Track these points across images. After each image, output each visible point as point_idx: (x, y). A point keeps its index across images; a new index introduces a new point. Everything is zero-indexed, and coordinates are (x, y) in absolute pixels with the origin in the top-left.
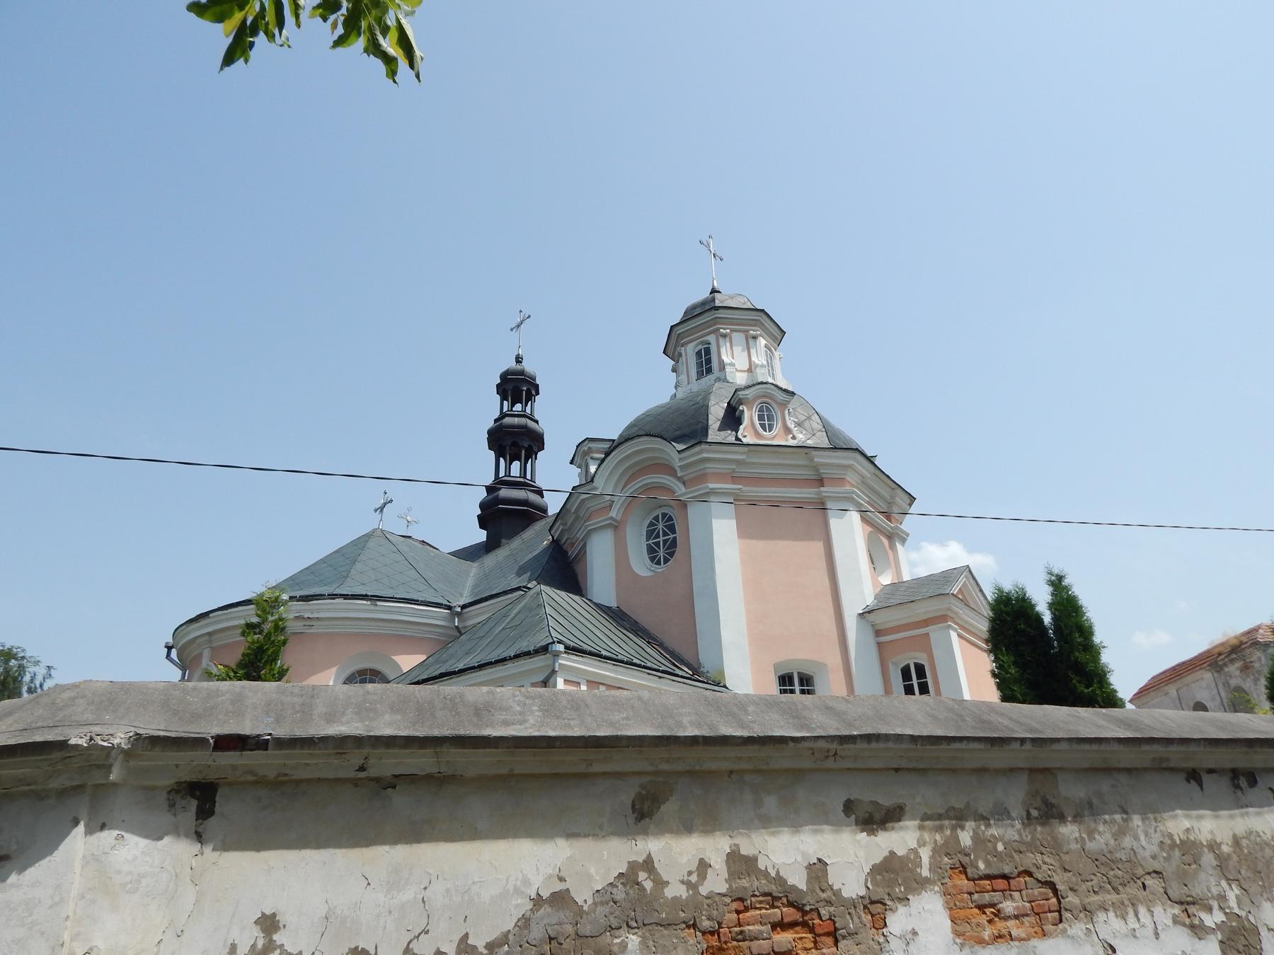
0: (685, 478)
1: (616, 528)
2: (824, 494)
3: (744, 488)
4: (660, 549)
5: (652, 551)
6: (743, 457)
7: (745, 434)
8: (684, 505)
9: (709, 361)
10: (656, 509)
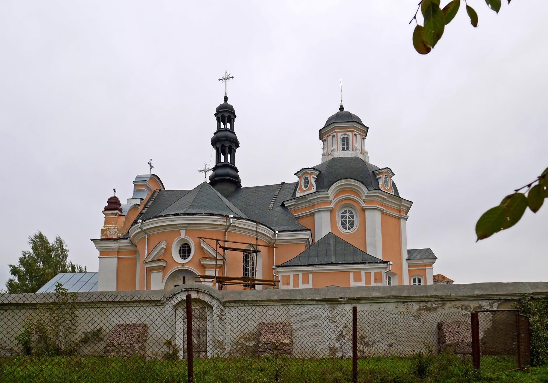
0: (365, 200)
1: (331, 211)
2: (364, 208)
3: (385, 210)
4: (347, 224)
5: (342, 223)
6: (386, 197)
7: (382, 187)
8: (364, 210)
9: (347, 144)
10: (345, 207)
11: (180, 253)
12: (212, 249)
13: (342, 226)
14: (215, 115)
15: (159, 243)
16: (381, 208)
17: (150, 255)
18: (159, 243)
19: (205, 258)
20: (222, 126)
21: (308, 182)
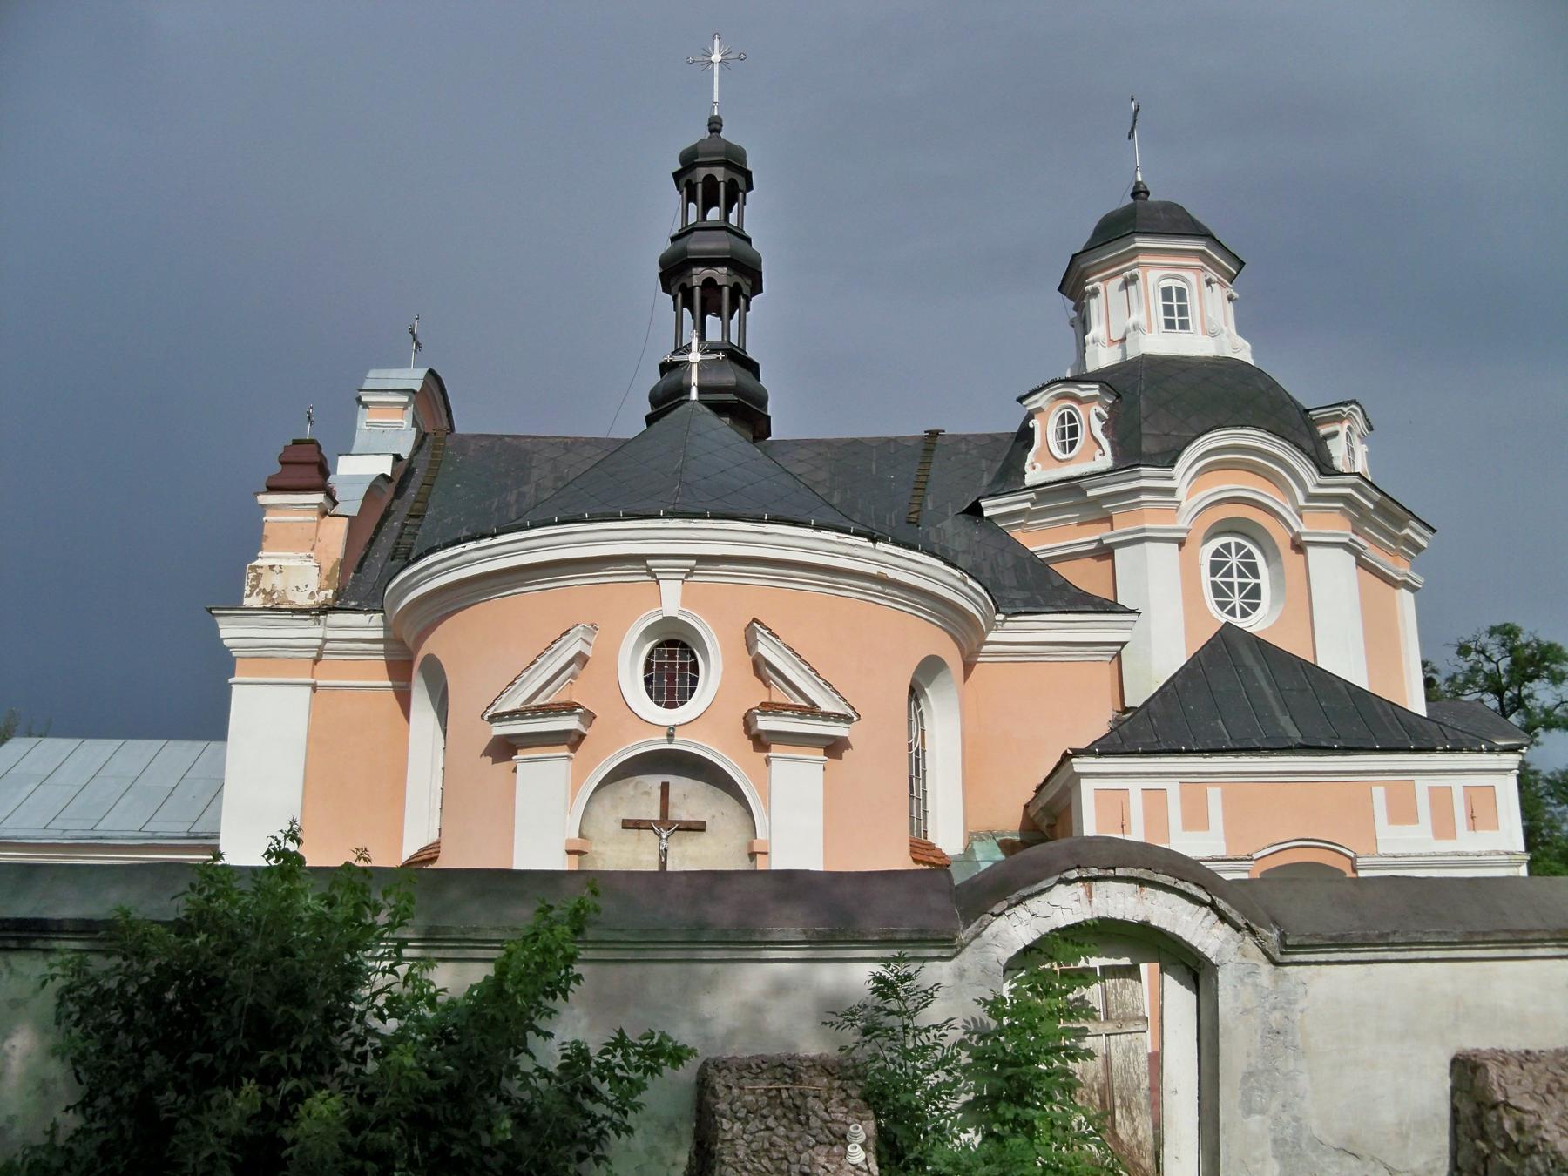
2: (1304, 538)
8: (1299, 547)
9: (1183, 311)
11: (648, 681)
12: (806, 668)
13: (1217, 602)
15: (566, 633)
16: (1359, 545)
17: (518, 682)
18: (566, 633)
19: (770, 708)
21: (1074, 432)
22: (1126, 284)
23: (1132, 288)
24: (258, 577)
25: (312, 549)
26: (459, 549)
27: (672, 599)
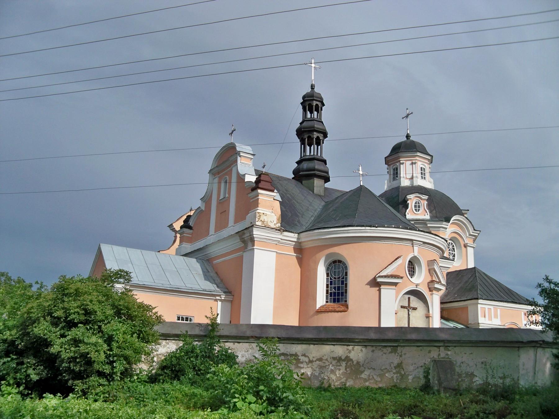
2: (468, 245)
8: (466, 246)
14: (302, 103)
20: (309, 115)
22: (412, 164)
23: (414, 165)
24: (260, 216)
25: (273, 210)
26: (363, 228)
27: (416, 251)
